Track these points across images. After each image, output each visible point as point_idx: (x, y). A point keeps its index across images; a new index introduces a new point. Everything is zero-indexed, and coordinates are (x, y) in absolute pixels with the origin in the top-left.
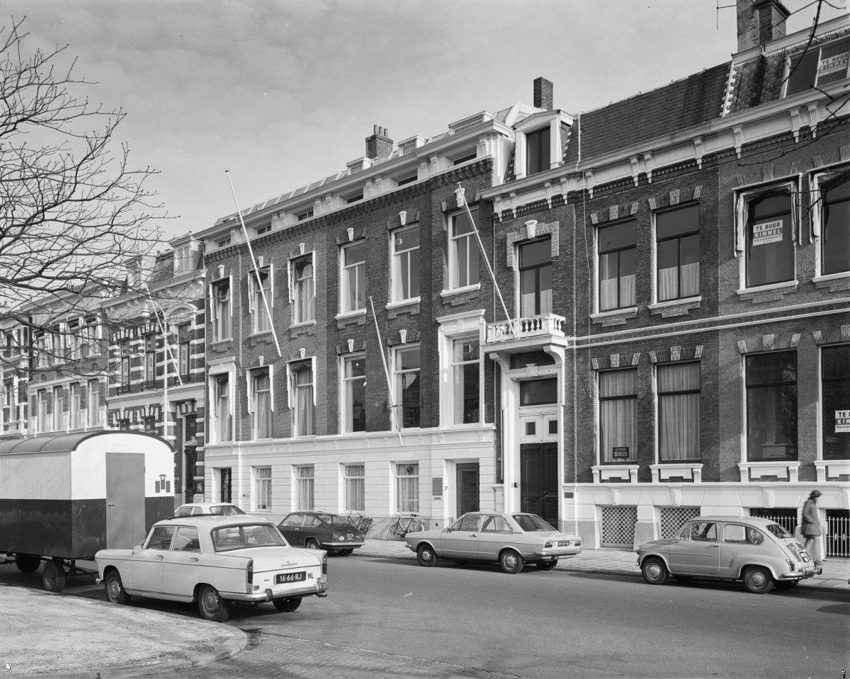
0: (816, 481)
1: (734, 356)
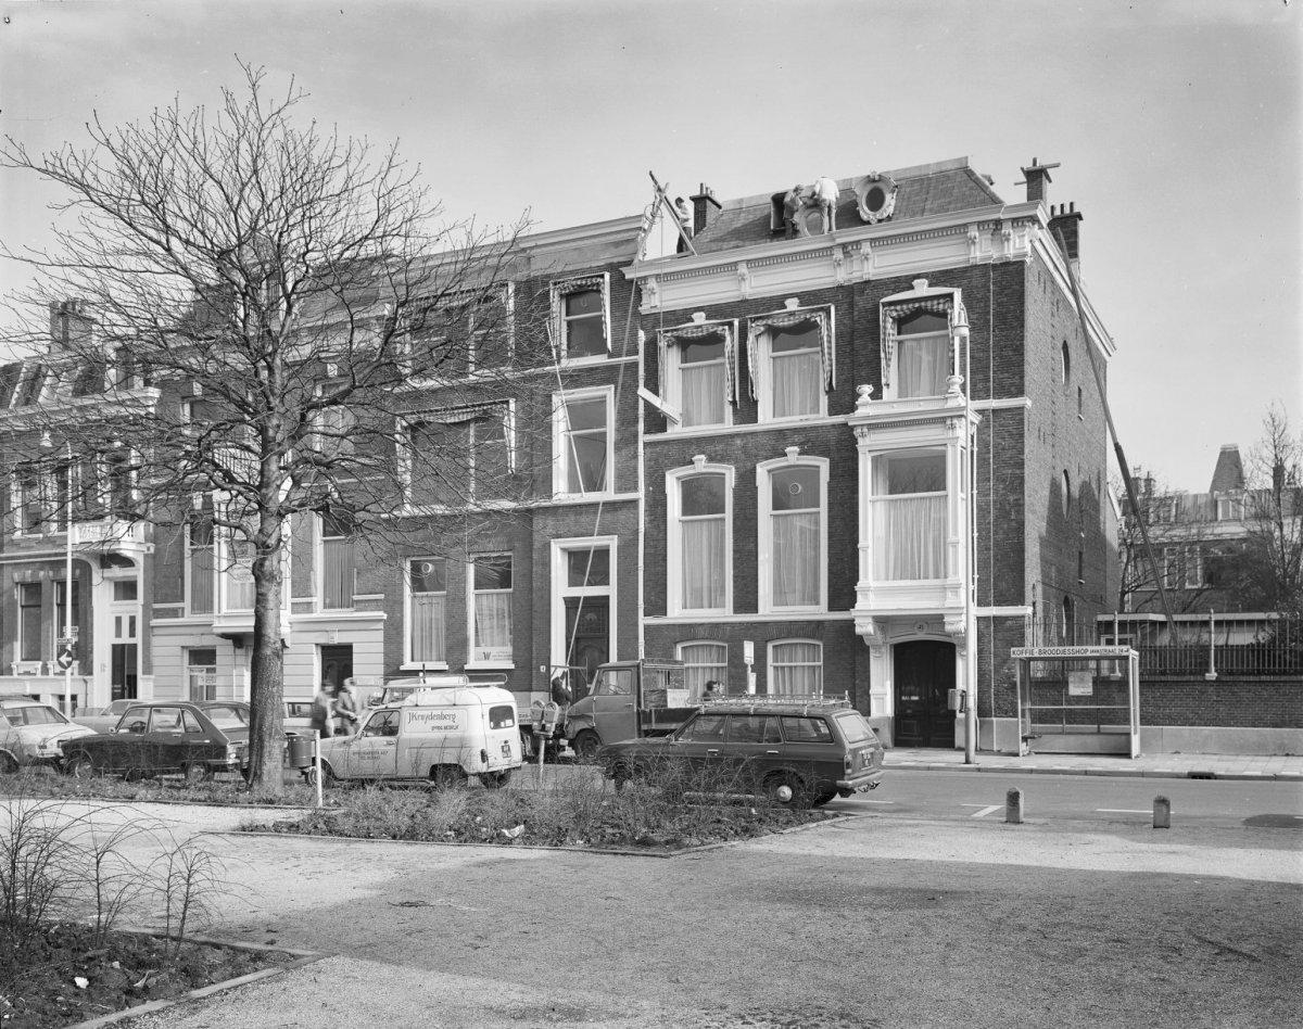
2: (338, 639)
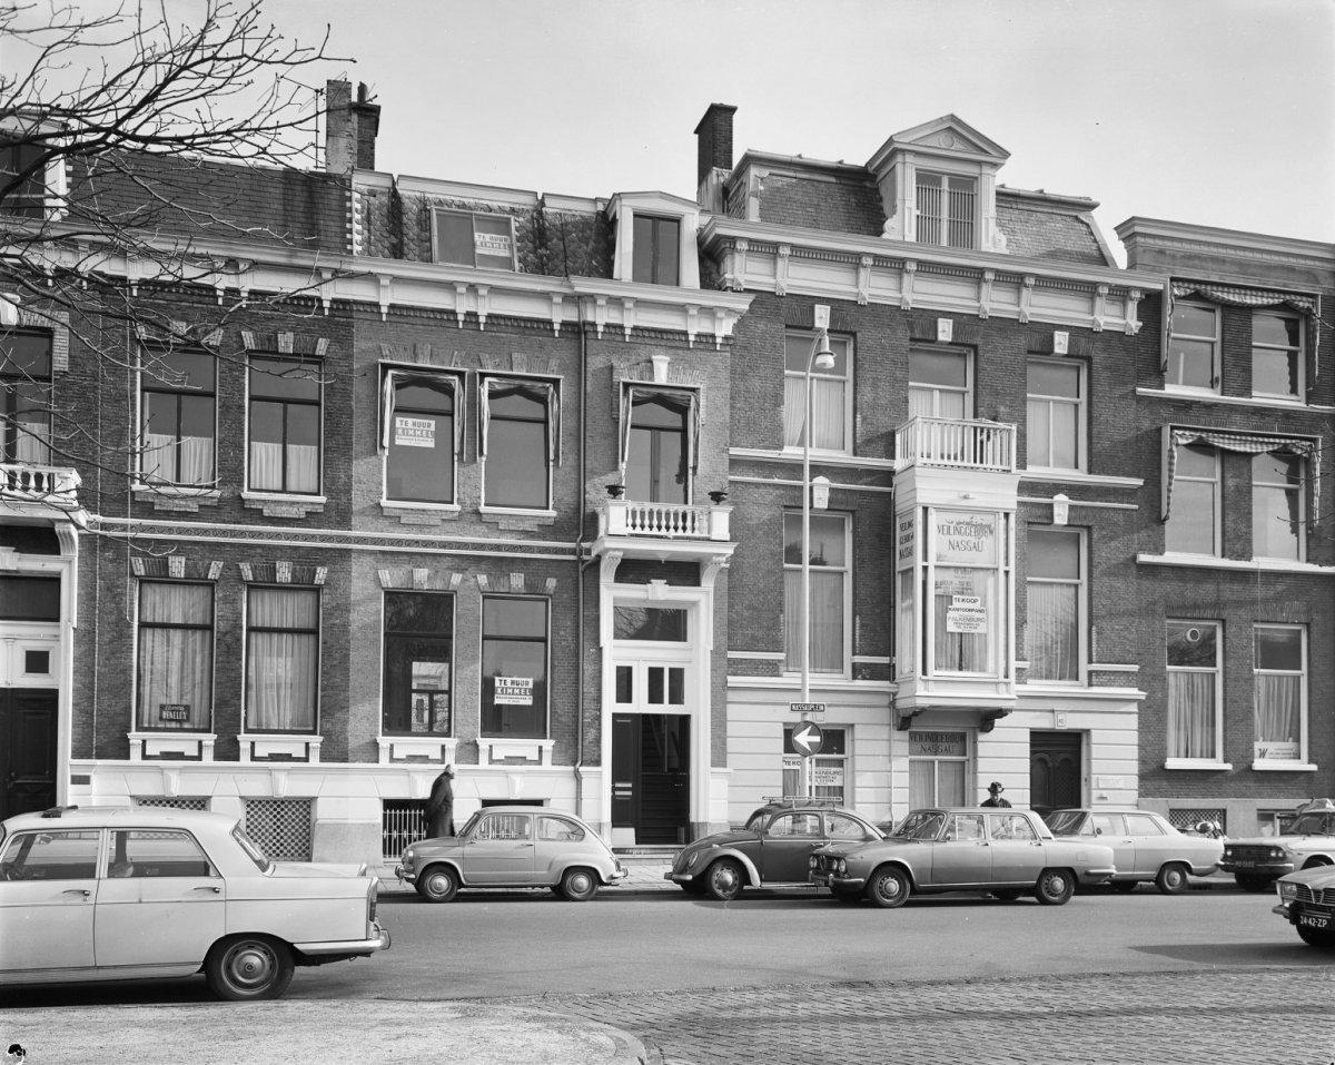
0: (477, 763)
1: (371, 588)
2: (1070, 722)
